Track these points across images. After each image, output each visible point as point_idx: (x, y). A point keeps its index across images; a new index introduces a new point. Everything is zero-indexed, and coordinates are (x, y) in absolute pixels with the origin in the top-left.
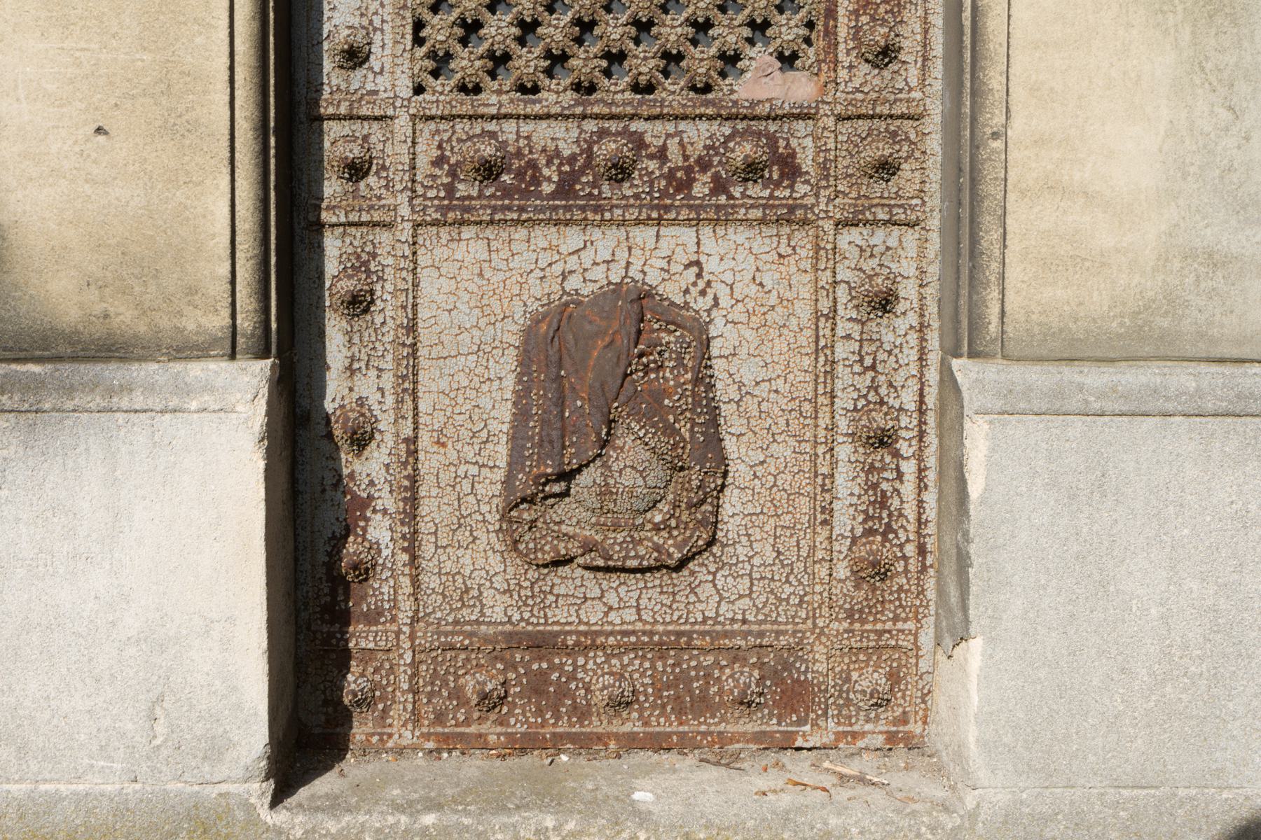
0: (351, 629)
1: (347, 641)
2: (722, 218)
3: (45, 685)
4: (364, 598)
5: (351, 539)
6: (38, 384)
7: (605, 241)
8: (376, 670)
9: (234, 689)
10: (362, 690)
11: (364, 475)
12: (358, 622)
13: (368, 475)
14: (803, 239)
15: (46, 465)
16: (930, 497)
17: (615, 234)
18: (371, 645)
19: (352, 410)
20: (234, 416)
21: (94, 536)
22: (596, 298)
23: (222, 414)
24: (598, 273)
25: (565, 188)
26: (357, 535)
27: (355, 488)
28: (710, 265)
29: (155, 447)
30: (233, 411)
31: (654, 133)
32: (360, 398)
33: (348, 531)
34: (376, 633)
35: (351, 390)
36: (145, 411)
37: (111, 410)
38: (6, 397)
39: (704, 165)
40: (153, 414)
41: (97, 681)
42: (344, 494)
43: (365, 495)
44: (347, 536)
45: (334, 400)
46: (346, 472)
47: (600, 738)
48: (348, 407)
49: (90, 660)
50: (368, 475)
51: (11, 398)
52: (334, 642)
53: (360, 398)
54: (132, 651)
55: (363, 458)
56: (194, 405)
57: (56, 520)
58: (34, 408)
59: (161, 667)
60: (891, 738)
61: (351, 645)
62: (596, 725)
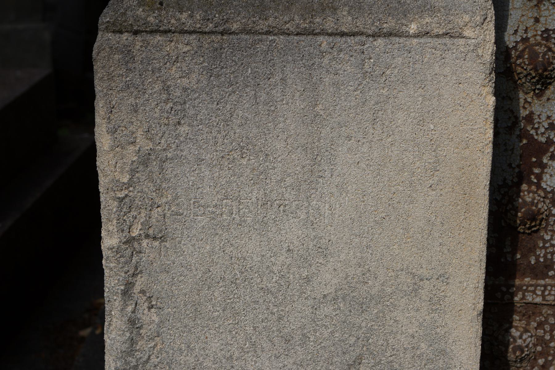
0: (517, 282)
1: (513, 295)
3: (227, 344)
4: (532, 250)
5: (524, 187)
8: (540, 325)
9: (443, 352)
10: (527, 346)
11: (543, 117)
12: (524, 275)
13: (549, 117)
15: (234, 97)
18: (538, 300)
19: (539, 44)
20: (462, 41)
21: (289, 181)
23: (447, 40)
26: (530, 183)
27: (533, 132)
29: (364, 78)
30: (461, 36)
32: (547, 30)
33: (521, 178)
34: (545, 286)
35: (537, 20)
36: (354, 34)
37: (313, 33)
38: (185, 15)
40: (364, 38)
41: (287, 341)
42: (520, 138)
43: (543, 140)
44: (520, 184)
45: (516, 31)
46: (524, 113)
48: (532, 41)
49: (280, 318)
50: (549, 117)
51: (191, 16)
52: (499, 295)
53: (547, 30)
54: (328, 309)
55: (545, 98)
56: (413, 28)
57: (244, 162)
58: (221, 29)
59: (360, 327)
61: (516, 299)
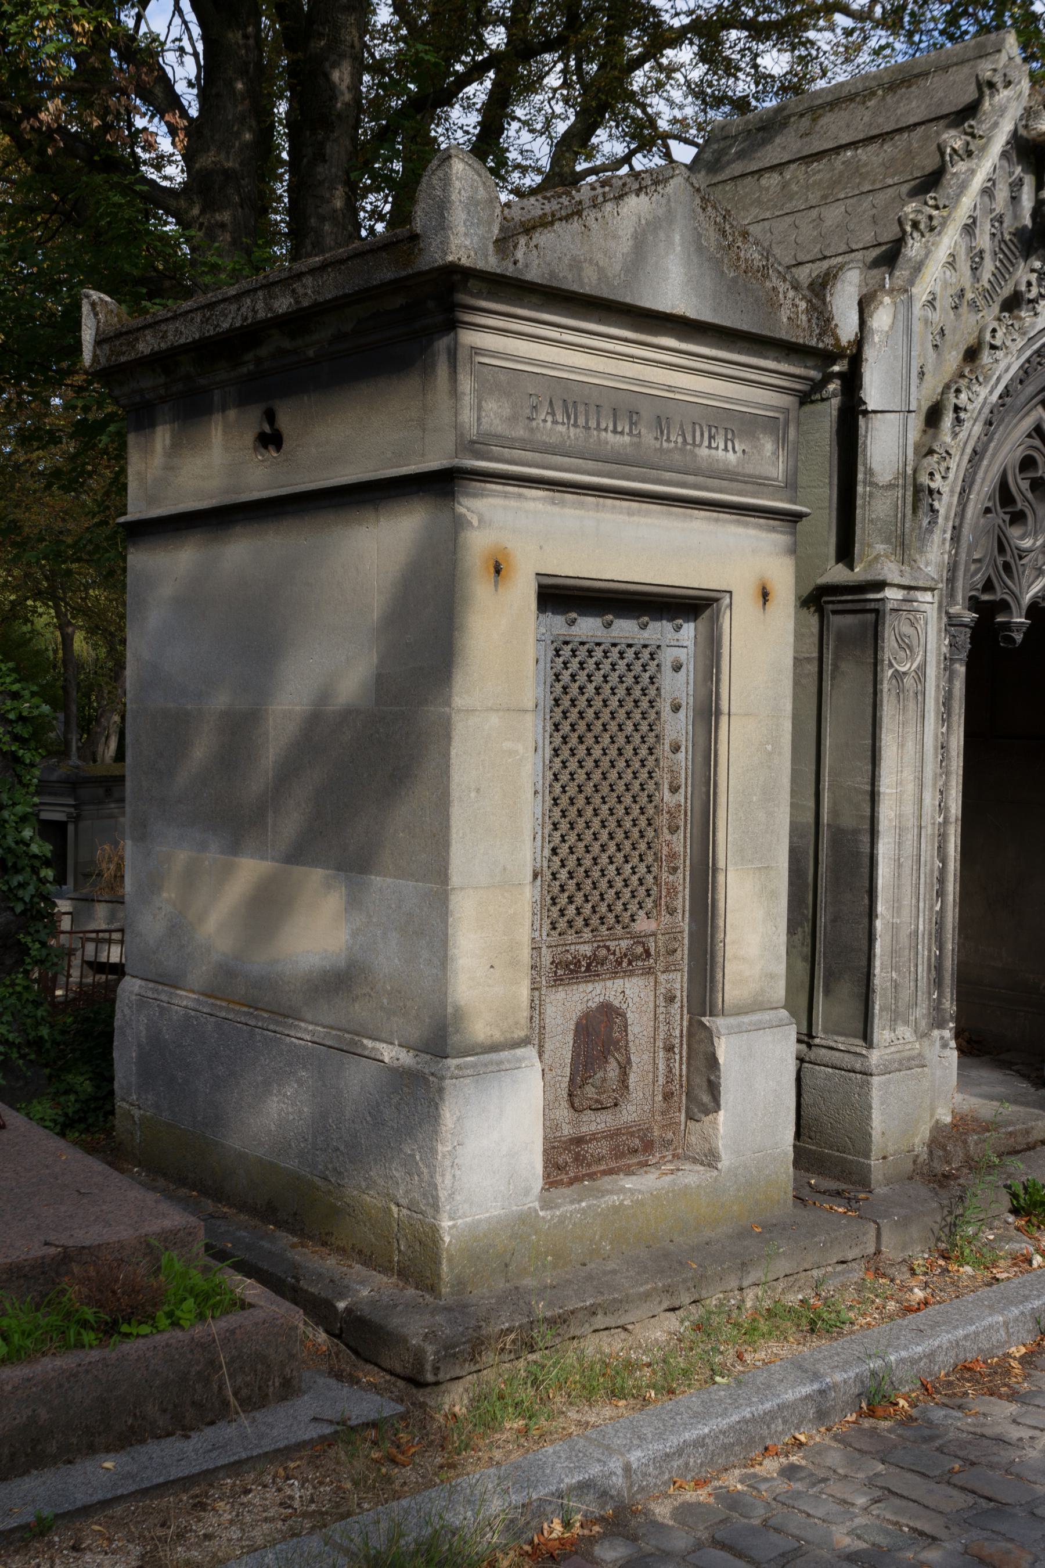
2: (631, 974)
6: (474, 1066)
7: (599, 987)
14: (652, 979)
16: (684, 1067)
17: (602, 983)
22: (597, 1008)
24: (597, 999)
25: (588, 969)
28: (627, 992)
31: (612, 945)
39: (625, 955)
47: (595, 1173)
60: (674, 1156)
62: (594, 1169)
